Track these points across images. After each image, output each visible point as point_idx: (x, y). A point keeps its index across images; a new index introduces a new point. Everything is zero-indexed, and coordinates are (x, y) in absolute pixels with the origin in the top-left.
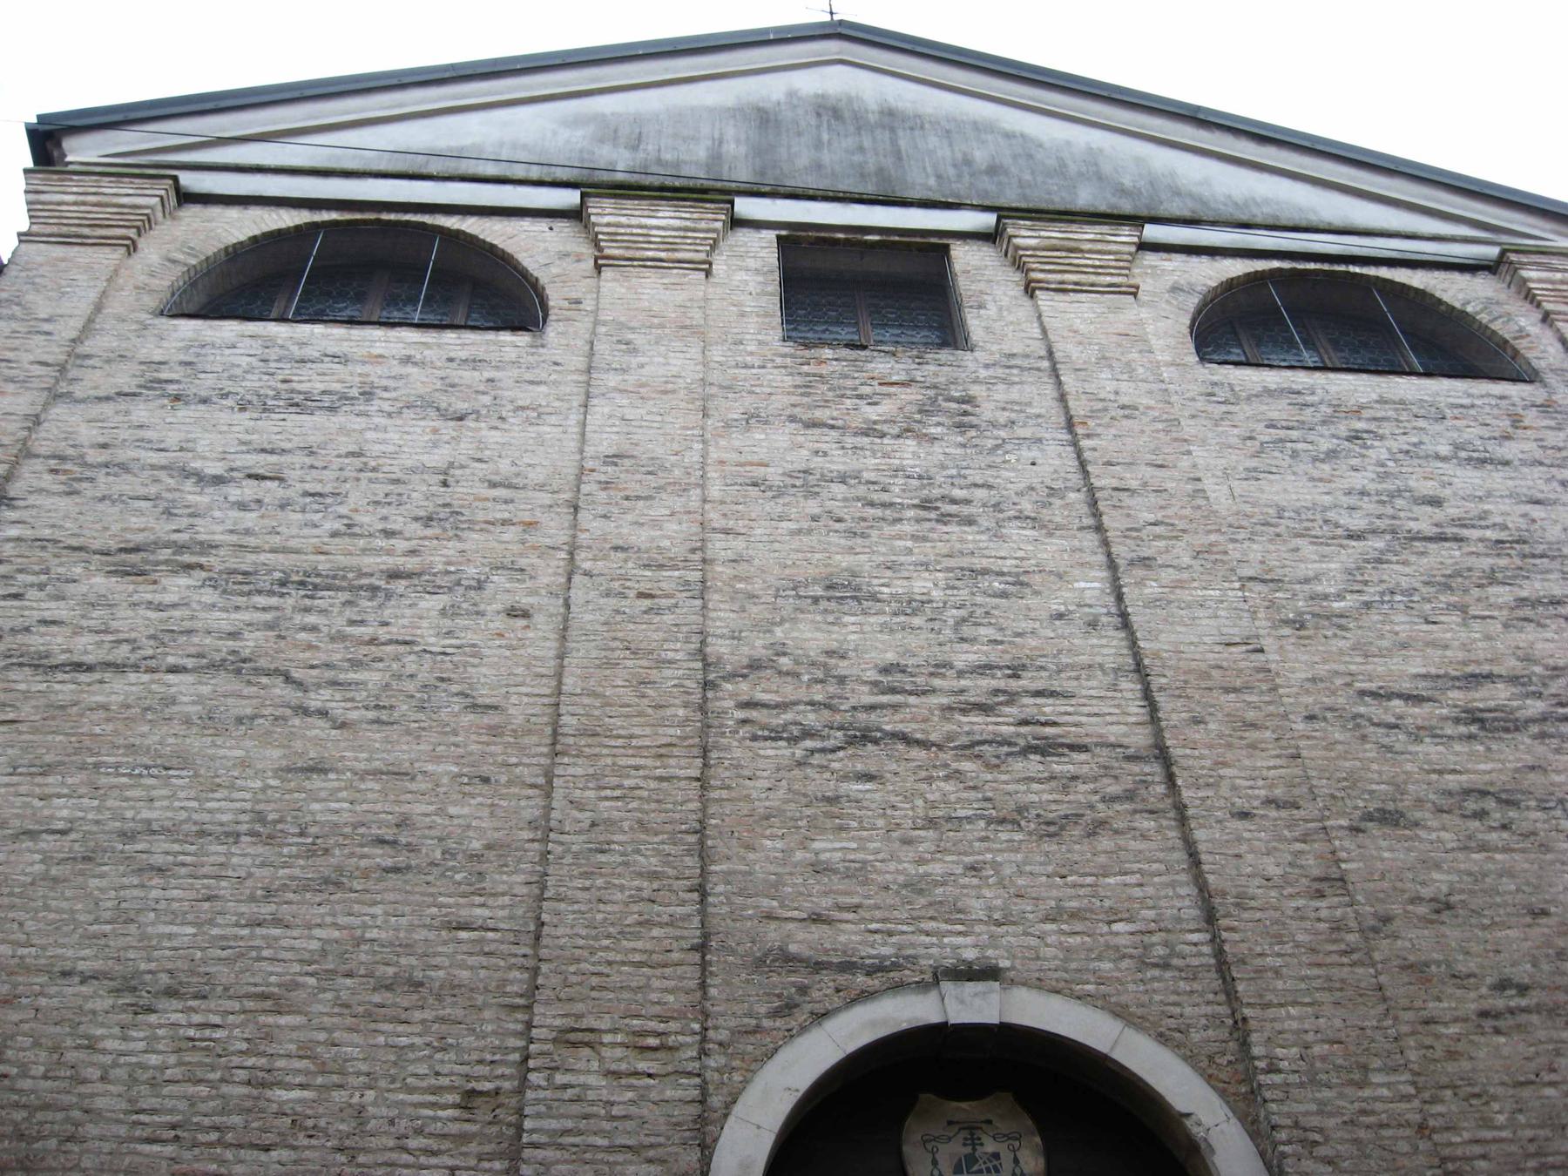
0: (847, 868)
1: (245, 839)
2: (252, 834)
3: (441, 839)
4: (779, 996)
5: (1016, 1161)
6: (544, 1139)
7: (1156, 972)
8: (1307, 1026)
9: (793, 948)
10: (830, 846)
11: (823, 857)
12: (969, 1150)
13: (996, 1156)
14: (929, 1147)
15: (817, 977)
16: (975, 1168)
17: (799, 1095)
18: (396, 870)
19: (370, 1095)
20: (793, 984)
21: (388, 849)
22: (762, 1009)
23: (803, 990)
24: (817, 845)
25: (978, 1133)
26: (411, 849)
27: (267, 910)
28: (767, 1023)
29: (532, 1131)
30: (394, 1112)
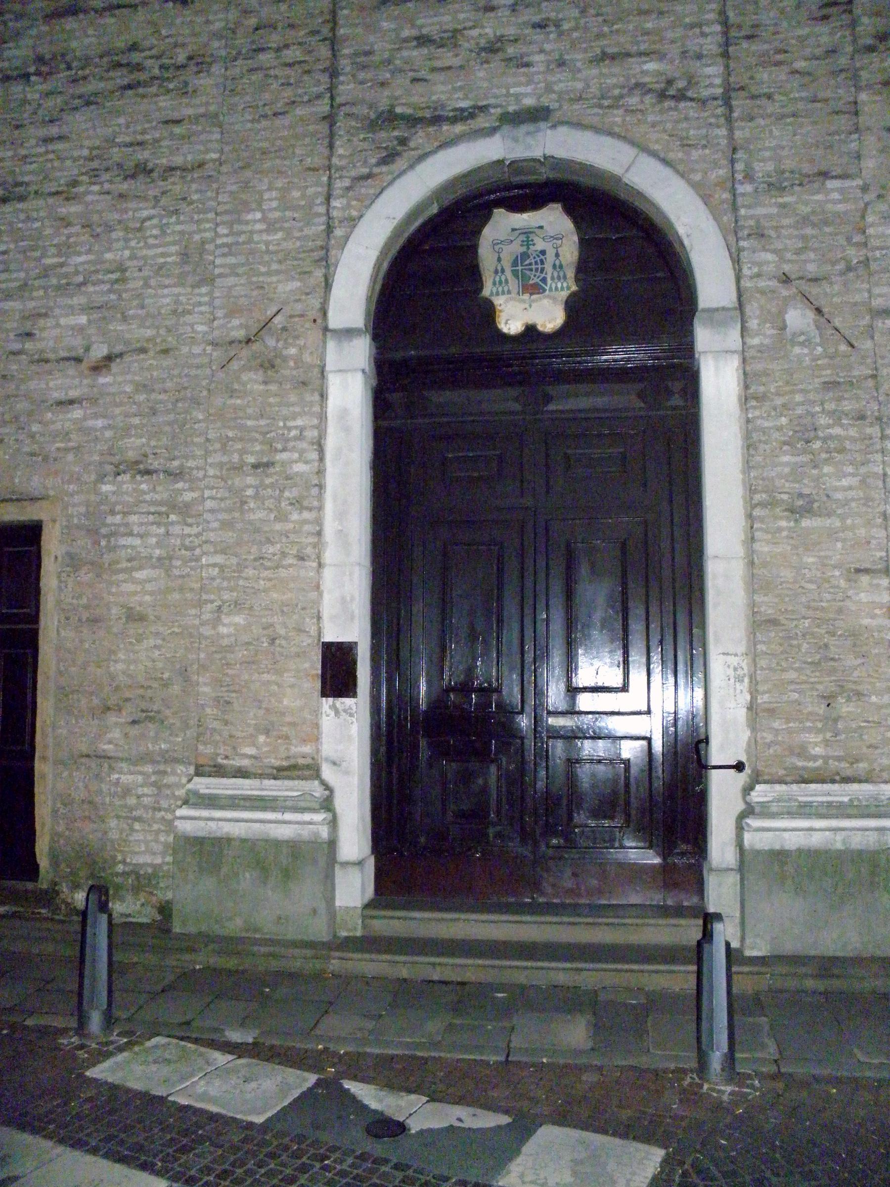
0: (441, 38)
1: (33, 78)
2: (38, 73)
3: (158, 57)
4: (386, 148)
5: (557, 255)
6: (227, 271)
7: (672, 103)
8: (784, 143)
9: (399, 110)
10: (429, 21)
11: (425, 31)
12: (524, 249)
13: (543, 252)
14: (497, 247)
15: (413, 130)
16: (527, 262)
17: (396, 222)
18: (129, 87)
19: (127, 253)
20: (397, 138)
21: (125, 71)
22: (373, 161)
23: (403, 141)
24: (419, 22)
25: (532, 236)
26: (139, 67)
27: (54, 130)
28: (376, 170)
29: (221, 266)
30: (142, 263)
